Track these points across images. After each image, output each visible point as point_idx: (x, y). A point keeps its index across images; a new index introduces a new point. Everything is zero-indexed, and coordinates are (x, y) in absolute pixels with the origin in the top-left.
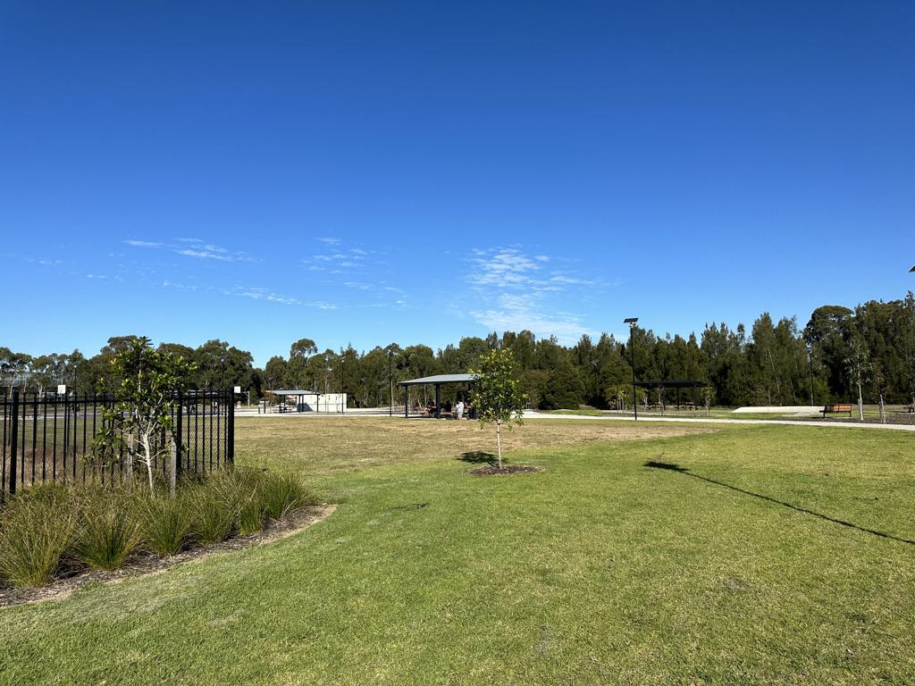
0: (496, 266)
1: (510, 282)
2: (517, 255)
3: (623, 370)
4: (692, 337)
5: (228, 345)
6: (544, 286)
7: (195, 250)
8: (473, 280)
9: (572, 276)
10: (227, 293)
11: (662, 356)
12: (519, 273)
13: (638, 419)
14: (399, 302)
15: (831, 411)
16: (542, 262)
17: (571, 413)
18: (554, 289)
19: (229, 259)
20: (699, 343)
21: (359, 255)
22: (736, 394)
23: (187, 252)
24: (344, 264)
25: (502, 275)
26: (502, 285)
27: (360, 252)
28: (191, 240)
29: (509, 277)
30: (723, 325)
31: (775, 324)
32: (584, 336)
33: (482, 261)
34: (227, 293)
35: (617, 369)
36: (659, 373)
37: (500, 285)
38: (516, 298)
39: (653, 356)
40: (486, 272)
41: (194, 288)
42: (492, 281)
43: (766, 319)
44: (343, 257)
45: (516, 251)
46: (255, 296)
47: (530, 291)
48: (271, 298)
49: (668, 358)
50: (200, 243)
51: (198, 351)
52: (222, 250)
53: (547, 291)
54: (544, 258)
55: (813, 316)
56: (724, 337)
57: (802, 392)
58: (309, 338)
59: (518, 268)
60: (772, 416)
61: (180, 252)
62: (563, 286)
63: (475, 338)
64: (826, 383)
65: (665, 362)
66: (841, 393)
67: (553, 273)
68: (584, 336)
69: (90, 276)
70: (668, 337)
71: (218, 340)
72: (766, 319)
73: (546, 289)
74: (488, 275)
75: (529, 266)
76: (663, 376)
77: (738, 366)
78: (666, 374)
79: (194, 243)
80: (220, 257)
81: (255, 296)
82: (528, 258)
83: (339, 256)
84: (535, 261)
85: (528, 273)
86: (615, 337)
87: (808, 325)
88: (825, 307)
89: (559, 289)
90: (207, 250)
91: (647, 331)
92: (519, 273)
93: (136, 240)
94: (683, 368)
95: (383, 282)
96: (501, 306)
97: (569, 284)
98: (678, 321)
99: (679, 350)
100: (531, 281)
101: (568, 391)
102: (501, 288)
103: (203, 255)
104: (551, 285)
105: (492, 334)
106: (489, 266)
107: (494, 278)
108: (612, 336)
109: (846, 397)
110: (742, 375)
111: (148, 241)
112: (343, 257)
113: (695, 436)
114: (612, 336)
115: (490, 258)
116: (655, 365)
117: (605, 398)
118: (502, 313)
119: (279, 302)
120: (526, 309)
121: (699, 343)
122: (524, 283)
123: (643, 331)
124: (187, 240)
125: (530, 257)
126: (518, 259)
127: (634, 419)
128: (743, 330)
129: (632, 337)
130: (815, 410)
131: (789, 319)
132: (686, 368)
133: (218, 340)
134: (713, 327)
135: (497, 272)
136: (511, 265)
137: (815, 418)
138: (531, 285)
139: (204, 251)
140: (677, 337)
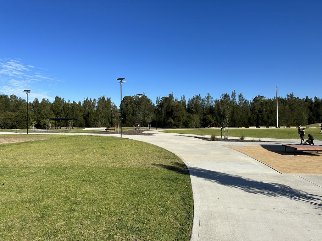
0: (8, 66)
1: (15, 74)
2: (18, 63)
3: (49, 113)
11: (66, 108)
12: (20, 71)
13: (29, 133)
15: (109, 129)
16: (31, 68)
17: (10, 132)
18: (36, 80)
20: (82, 104)
25: (11, 71)
26: (11, 75)
29: (14, 72)
31: (106, 99)
32: (36, 99)
33: (1, 63)
35: (47, 113)
36: (64, 115)
37: (10, 75)
38: (18, 82)
39: (63, 108)
42: (5, 73)
43: (103, 98)
45: (18, 61)
47: (25, 80)
53: (33, 80)
54: (32, 67)
56: (90, 103)
59: (19, 69)
60: (89, 131)
62: (40, 79)
67: (37, 73)
68: (36, 99)
72: (103, 98)
74: (4, 70)
75: (24, 69)
76: (66, 116)
77: (93, 113)
84: (28, 67)
85: (24, 71)
88: (127, 96)
89: (38, 80)
91: (62, 98)
92: (20, 71)
94: (73, 113)
96: (10, 84)
97: (43, 79)
98: (74, 96)
100: (26, 75)
101: (24, 121)
102: (11, 76)
104: (35, 78)
106: (4, 66)
108: (48, 99)
109: (125, 124)
110: (94, 117)
113: (40, 141)
114: (48, 99)
115: (5, 63)
116: (63, 111)
118: (11, 87)
121: (82, 104)
122: (22, 75)
123: (60, 99)
125: (26, 65)
126: (19, 65)
127: (119, 136)
130: (104, 129)
132: (75, 113)
134: (87, 99)
137: (103, 132)
138: (26, 77)
140: (74, 102)
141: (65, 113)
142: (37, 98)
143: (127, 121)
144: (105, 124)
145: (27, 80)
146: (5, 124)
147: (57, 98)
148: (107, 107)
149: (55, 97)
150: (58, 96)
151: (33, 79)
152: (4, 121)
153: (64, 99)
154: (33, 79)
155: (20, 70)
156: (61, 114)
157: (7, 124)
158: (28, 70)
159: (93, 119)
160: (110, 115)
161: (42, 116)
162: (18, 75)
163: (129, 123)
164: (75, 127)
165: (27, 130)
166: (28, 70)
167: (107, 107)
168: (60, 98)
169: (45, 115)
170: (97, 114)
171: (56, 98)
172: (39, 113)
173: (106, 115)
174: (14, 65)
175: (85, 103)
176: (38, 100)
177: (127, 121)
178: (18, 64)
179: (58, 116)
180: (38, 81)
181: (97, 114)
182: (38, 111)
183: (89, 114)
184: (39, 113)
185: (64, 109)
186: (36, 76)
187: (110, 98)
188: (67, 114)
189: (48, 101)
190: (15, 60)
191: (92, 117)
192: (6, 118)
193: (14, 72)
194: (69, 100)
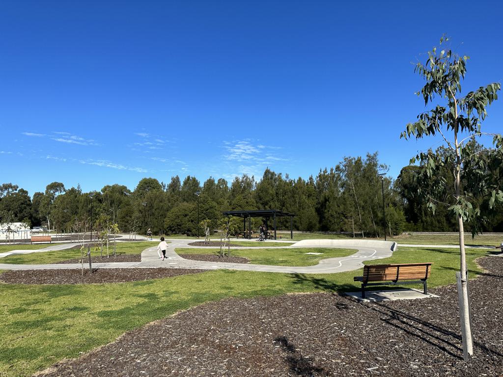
0: (236, 150)
1: (244, 159)
2: (247, 145)
3: (247, 202)
4: (311, 178)
5: (18, 187)
6: (263, 161)
7: (65, 139)
8: (224, 157)
9: (277, 157)
10: (84, 163)
12: (249, 154)
14: (183, 169)
16: (261, 149)
18: (268, 163)
19: (85, 144)
24: (151, 148)
26: (240, 160)
28: (63, 133)
29: (243, 156)
33: (230, 147)
34: (84, 163)
36: (278, 204)
37: (239, 161)
40: (231, 153)
41: (65, 160)
42: (234, 158)
44: (151, 144)
45: (246, 143)
46: (100, 165)
47: (255, 164)
48: (109, 166)
50: (68, 135)
52: (81, 139)
53: (264, 164)
54: (262, 147)
55: (401, 172)
57: (380, 221)
58: (59, 181)
59: (248, 152)
61: (56, 139)
62: (272, 162)
63: (150, 178)
64: (402, 213)
66: (416, 222)
67: (267, 155)
70: (287, 177)
71: (10, 184)
74: (232, 155)
75: (254, 150)
81: (100, 165)
82: (253, 146)
84: (257, 148)
85: (254, 154)
87: (398, 177)
90: (72, 139)
92: (249, 154)
95: (173, 158)
96: (239, 172)
97: (275, 160)
99: (297, 189)
103: (70, 141)
107: (236, 157)
108: (253, 177)
109: (420, 224)
112: (151, 144)
114: (253, 177)
115: (233, 146)
123: (273, 174)
124: (61, 133)
125: (254, 145)
126: (248, 147)
131: (372, 155)
132: (297, 201)
133: (10, 184)
134: (325, 171)
135: (238, 153)
138: (255, 161)
139: (70, 139)
143: (426, 214)
144: (363, 226)
145: (258, 164)
146: (178, 225)
147: (267, 172)
148: (368, 178)
151: (264, 163)
153: (281, 174)
154: (264, 163)
157: (180, 225)
159: (336, 212)
160: (376, 200)
162: (247, 160)
163: (432, 222)
164: (298, 230)
167: (368, 178)
168: (274, 173)
171: (265, 173)
173: (365, 202)
174: (242, 148)
175: (321, 180)
177: (426, 214)
179: (266, 206)
183: (326, 200)
186: (268, 158)
187: (375, 155)
189: (254, 180)
191: (333, 210)
193: (243, 156)
194: (287, 174)
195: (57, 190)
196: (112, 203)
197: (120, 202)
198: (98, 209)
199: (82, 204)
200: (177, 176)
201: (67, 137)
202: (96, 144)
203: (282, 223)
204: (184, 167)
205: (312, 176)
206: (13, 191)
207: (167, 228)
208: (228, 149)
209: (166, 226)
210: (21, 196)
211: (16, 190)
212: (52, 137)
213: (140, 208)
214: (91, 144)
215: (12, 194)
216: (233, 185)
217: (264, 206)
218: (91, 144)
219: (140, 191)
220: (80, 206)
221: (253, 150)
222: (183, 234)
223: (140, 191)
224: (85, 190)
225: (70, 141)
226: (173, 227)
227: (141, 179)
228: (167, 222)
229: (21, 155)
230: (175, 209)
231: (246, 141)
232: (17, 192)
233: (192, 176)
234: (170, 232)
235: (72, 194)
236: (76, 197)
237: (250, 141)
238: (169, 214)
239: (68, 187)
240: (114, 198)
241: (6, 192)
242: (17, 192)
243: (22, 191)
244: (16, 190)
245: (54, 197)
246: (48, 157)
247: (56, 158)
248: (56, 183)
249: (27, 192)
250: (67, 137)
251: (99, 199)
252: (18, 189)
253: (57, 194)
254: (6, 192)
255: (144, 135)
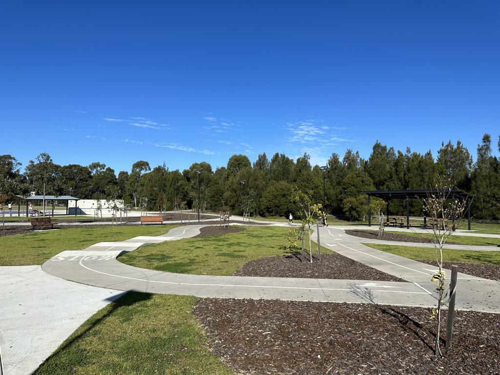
0: (299, 132)
1: (307, 141)
2: (311, 126)
3: (363, 181)
4: (429, 154)
5: (105, 166)
7: (140, 123)
10: (158, 145)
12: (313, 136)
13: (200, 221)
16: (325, 130)
18: (332, 144)
21: (227, 126)
22: (480, 207)
23: (136, 125)
26: (303, 142)
27: (226, 124)
30: (459, 143)
32: (334, 155)
34: (158, 145)
35: (357, 181)
37: (302, 142)
39: (394, 169)
41: (141, 143)
42: (297, 140)
45: (310, 124)
46: (172, 147)
48: (180, 148)
49: (409, 170)
50: (144, 120)
51: (63, 167)
52: (155, 123)
53: (328, 146)
54: (326, 128)
58: (145, 160)
59: (312, 133)
61: (133, 124)
62: (337, 143)
63: (240, 155)
65: (404, 175)
67: (331, 136)
69: (88, 136)
70: (408, 151)
73: (327, 144)
74: (295, 137)
78: (406, 187)
79: (141, 120)
80: (153, 127)
81: (172, 147)
83: (215, 127)
84: (321, 129)
85: (318, 135)
86: (360, 154)
90: (147, 124)
91: (388, 148)
92: (313, 136)
93: (110, 118)
94: (423, 180)
97: (340, 141)
100: (319, 140)
102: (303, 144)
103: (145, 126)
104: (331, 142)
105: (262, 154)
107: (299, 139)
108: (357, 153)
111: (117, 119)
114: (357, 153)
115: (296, 128)
116: (395, 177)
117: (343, 208)
119: (184, 151)
120: (316, 155)
122: (315, 141)
123: (384, 148)
125: (318, 126)
126: (312, 128)
128: (489, 141)
129: (374, 153)
132: (426, 179)
135: (300, 135)
136: (308, 131)
138: (319, 142)
139: (145, 124)
141: (400, 180)
142: (335, 154)
145: (321, 146)
146: (276, 206)
147: (377, 147)
149: (373, 145)
150: (379, 142)
152: (274, 201)
155: (312, 134)
156: (391, 184)
157: (278, 207)
158: (321, 133)
161: (345, 189)
162: (311, 141)
165: (458, 308)
166: (321, 133)
169: (354, 185)
170: (496, 178)
171: (374, 148)
172: (339, 183)
174: (305, 130)
176: (336, 156)
178: (310, 128)
180: (334, 146)
181: (496, 178)
182: (338, 180)
184: (339, 183)
185: (397, 171)
186: (332, 139)
188: (406, 182)
189: (359, 157)
190: (307, 122)
192: (278, 195)
193: (306, 138)
194: (408, 148)
195: (142, 169)
196: (201, 181)
197: (210, 181)
198: (187, 187)
199: (170, 182)
200: (264, 153)
201: (142, 122)
202: (168, 128)
203: (405, 207)
204: (248, 150)
205: (430, 151)
206: (101, 169)
207: (265, 209)
208: (291, 130)
209: (263, 207)
210: (109, 174)
211: (104, 168)
212: (130, 122)
213: (234, 187)
214: (164, 128)
215: (100, 172)
216: (28, 168)
217: (262, 189)
218: (164, 128)
219: (231, 168)
220: (168, 184)
221: (317, 131)
222: (281, 216)
223: (231, 168)
224: (171, 168)
225: (145, 126)
226: (271, 208)
227: (230, 157)
228: (264, 202)
229: (104, 139)
230: (271, 188)
231: (309, 122)
232: (105, 170)
233: (280, 153)
234: (267, 214)
235: (159, 172)
236: (163, 175)
237: (313, 123)
238: (265, 194)
239: (153, 166)
240: (200, 175)
241: (95, 170)
242: (105, 170)
243: (109, 169)
244: (104, 168)
245: (140, 176)
246: (127, 141)
247: (134, 142)
248: (141, 162)
249: (113, 171)
250: (142, 122)
251: (187, 177)
252: (105, 168)
253: (143, 172)
254: (95, 170)
255: (210, 119)
